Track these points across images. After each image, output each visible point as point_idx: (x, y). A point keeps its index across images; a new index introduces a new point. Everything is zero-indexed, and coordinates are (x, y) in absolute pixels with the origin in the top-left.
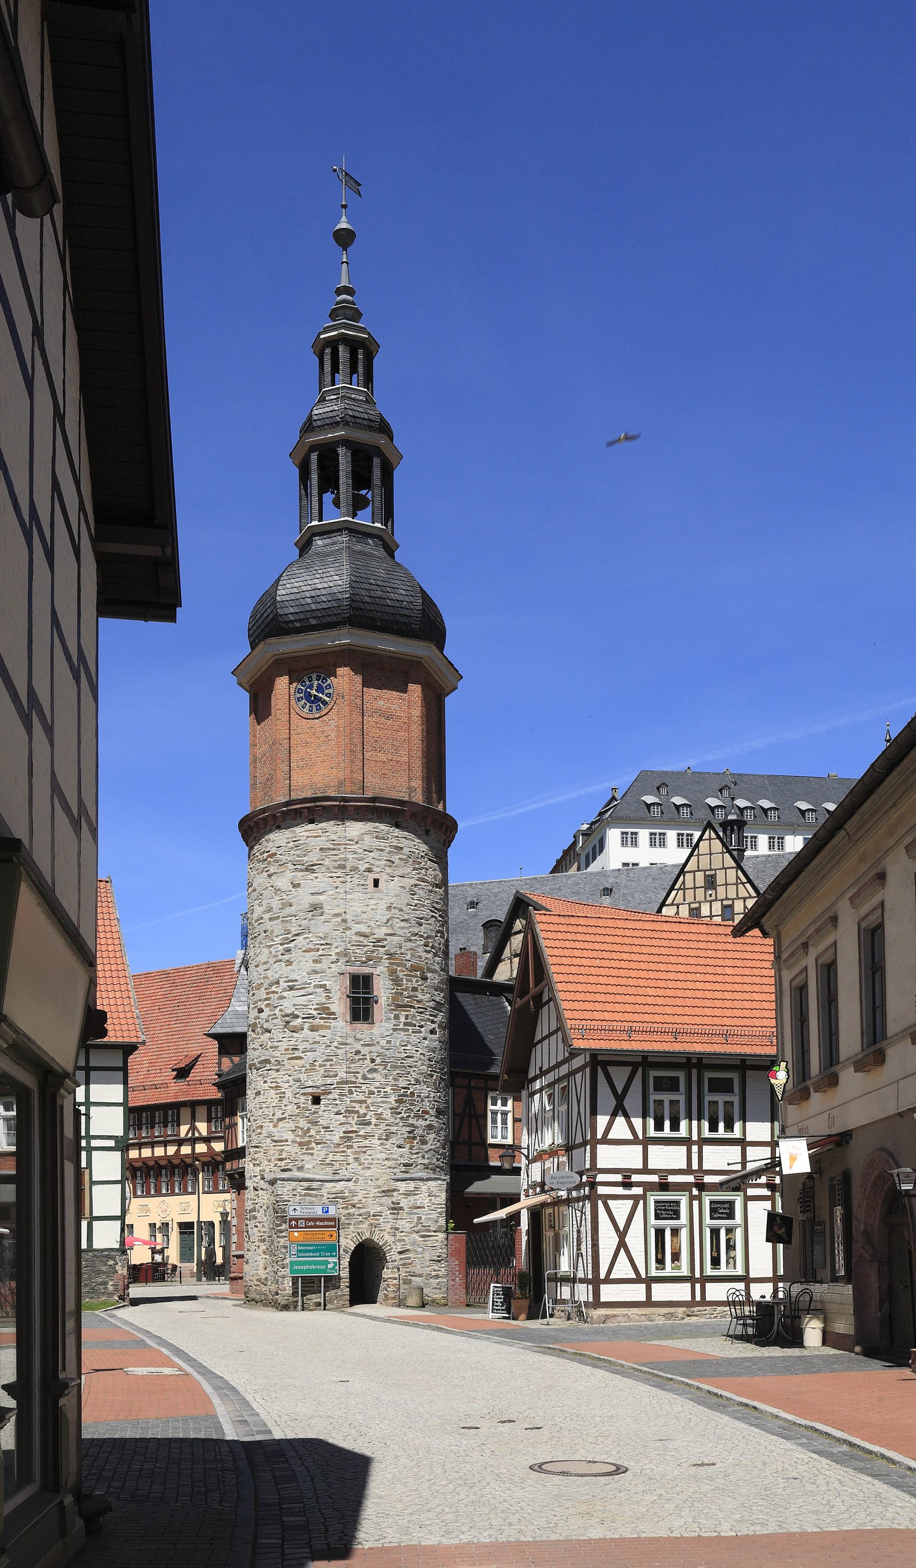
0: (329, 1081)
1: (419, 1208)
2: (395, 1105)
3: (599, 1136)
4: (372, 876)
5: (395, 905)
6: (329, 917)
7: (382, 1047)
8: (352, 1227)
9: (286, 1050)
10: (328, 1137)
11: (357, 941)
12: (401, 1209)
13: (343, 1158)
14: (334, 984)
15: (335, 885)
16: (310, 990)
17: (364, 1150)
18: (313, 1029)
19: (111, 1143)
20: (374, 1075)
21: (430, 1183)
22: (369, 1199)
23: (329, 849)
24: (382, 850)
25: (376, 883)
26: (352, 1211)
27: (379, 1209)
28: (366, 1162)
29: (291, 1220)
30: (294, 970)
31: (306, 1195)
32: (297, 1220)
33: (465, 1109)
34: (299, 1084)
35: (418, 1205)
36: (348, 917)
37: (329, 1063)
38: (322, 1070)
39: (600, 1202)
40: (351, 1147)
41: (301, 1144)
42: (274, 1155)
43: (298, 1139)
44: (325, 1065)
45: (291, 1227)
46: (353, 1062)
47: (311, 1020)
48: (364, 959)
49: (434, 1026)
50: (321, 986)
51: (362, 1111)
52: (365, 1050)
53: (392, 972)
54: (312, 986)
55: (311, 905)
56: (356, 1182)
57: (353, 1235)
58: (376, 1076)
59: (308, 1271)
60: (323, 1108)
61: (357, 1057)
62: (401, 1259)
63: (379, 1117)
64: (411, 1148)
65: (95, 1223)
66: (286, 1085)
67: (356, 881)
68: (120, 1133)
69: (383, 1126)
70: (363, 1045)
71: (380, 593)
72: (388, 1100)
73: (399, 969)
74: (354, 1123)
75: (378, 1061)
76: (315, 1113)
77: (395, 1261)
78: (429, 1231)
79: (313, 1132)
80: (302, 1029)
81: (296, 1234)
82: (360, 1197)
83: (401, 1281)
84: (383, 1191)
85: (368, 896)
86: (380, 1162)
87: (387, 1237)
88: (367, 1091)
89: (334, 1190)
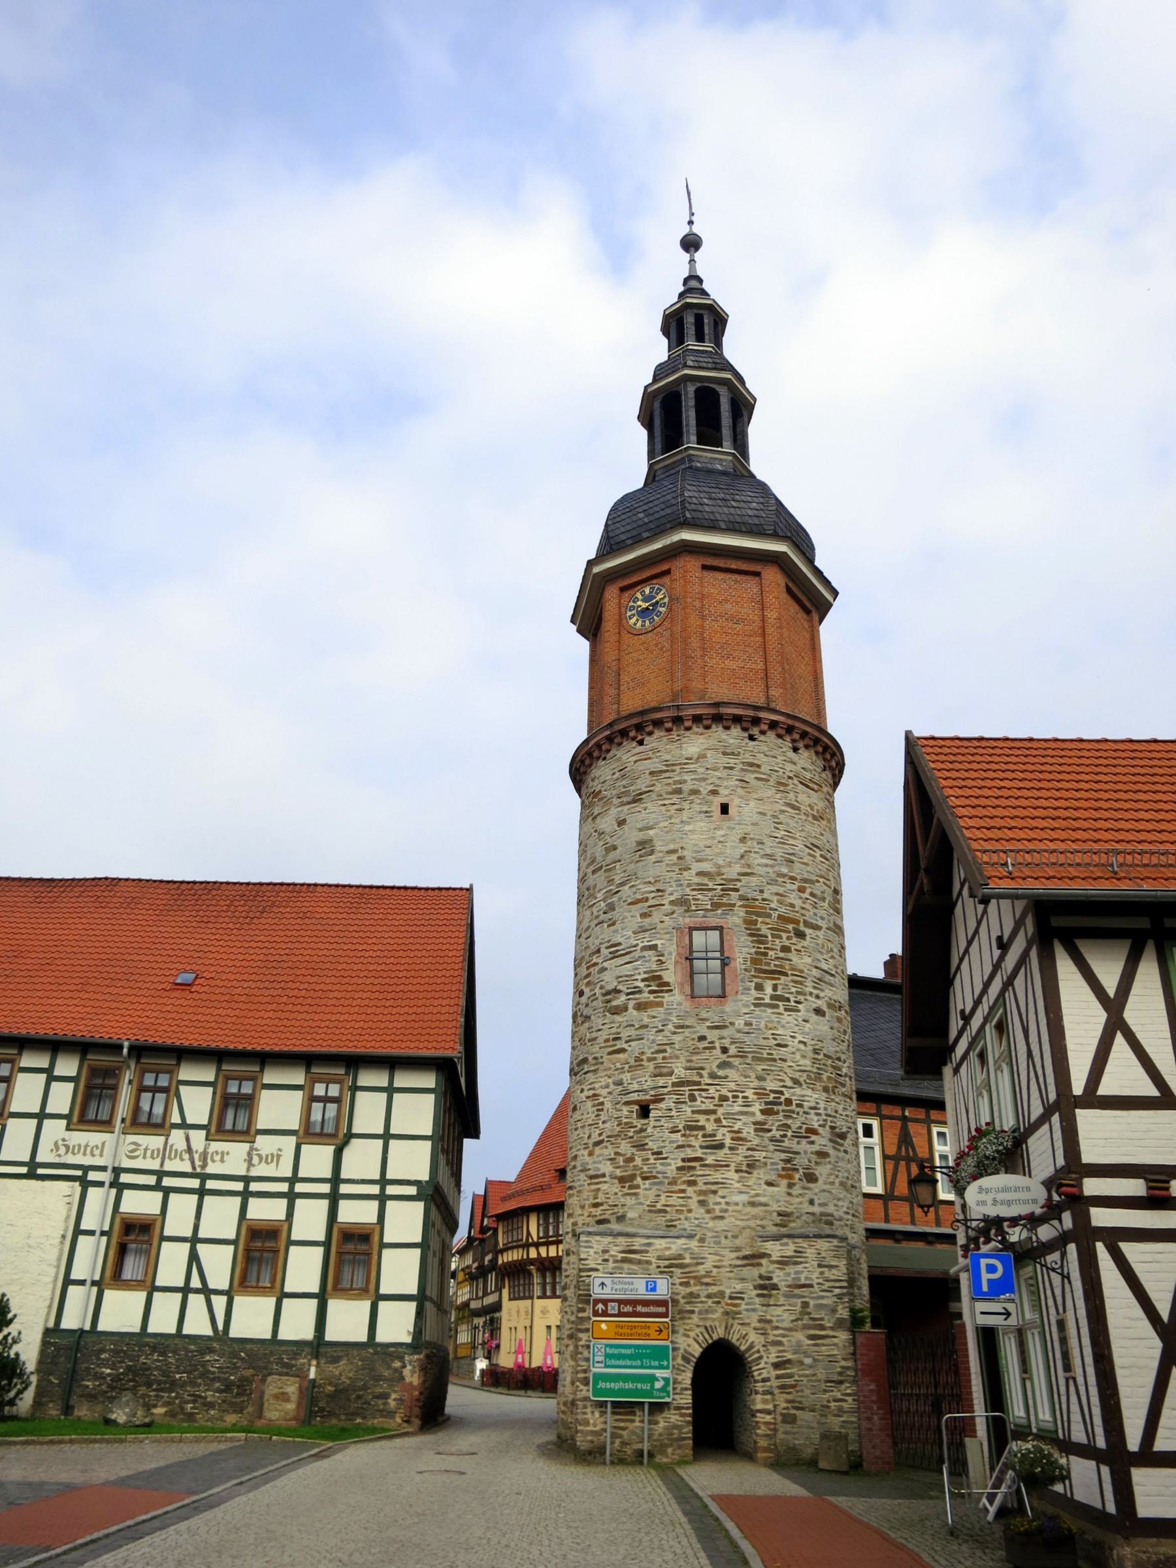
0: (661, 1081)
1: (804, 1286)
2: (760, 1117)
3: (1078, 1088)
4: (717, 801)
7: (739, 1031)
8: (695, 1317)
9: (607, 1041)
10: (660, 1168)
11: (698, 884)
12: (775, 1287)
13: (681, 1201)
14: (668, 944)
16: (637, 954)
17: (714, 1188)
18: (640, 1007)
19: (412, 1190)
22: (722, 1270)
23: (662, 772)
24: (731, 768)
25: (725, 809)
26: (695, 1289)
27: (739, 1287)
28: (717, 1208)
29: (596, 1302)
30: (617, 931)
31: (624, 1260)
32: (605, 1302)
33: (899, 1148)
34: (620, 1088)
35: (803, 1281)
36: (685, 853)
37: (661, 1055)
38: (651, 1066)
39: (1100, 1246)
41: (622, 1180)
42: (588, 1199)
43: (618, 1173)
44: (655, 1059)
45: (596, 1314)
46: (696, 1052)
47: (637, 996)
49: (819, 1002)
52: (712, 1035)
53: (750, 923)
54: (638, 948)
56: (702, 1240)
57: (698, 1331)
59: (621, 1392)
60: (652, 1123)
62: (778, 1377)
63: (738, 1138)
64: (790, 1186)
65: (285, 1301)
66: (604, 1092)
67: (697, 808)
68: (424, 1176)
69: (742, 1150)
70: (709, 1027)
72: (749, 1109)
73: (760, 920)
75: (733, 1050)
78: (822, 1328)
79: (638, 1161)
80: (626, 1009)
81: (604, 1326)
82: (708, 1265)
83: (779, 1418)
84: (745, 1258)
86: (739, 1208)
87: (753, 1337)
88: (716, 1095)
89: (667, 1253)
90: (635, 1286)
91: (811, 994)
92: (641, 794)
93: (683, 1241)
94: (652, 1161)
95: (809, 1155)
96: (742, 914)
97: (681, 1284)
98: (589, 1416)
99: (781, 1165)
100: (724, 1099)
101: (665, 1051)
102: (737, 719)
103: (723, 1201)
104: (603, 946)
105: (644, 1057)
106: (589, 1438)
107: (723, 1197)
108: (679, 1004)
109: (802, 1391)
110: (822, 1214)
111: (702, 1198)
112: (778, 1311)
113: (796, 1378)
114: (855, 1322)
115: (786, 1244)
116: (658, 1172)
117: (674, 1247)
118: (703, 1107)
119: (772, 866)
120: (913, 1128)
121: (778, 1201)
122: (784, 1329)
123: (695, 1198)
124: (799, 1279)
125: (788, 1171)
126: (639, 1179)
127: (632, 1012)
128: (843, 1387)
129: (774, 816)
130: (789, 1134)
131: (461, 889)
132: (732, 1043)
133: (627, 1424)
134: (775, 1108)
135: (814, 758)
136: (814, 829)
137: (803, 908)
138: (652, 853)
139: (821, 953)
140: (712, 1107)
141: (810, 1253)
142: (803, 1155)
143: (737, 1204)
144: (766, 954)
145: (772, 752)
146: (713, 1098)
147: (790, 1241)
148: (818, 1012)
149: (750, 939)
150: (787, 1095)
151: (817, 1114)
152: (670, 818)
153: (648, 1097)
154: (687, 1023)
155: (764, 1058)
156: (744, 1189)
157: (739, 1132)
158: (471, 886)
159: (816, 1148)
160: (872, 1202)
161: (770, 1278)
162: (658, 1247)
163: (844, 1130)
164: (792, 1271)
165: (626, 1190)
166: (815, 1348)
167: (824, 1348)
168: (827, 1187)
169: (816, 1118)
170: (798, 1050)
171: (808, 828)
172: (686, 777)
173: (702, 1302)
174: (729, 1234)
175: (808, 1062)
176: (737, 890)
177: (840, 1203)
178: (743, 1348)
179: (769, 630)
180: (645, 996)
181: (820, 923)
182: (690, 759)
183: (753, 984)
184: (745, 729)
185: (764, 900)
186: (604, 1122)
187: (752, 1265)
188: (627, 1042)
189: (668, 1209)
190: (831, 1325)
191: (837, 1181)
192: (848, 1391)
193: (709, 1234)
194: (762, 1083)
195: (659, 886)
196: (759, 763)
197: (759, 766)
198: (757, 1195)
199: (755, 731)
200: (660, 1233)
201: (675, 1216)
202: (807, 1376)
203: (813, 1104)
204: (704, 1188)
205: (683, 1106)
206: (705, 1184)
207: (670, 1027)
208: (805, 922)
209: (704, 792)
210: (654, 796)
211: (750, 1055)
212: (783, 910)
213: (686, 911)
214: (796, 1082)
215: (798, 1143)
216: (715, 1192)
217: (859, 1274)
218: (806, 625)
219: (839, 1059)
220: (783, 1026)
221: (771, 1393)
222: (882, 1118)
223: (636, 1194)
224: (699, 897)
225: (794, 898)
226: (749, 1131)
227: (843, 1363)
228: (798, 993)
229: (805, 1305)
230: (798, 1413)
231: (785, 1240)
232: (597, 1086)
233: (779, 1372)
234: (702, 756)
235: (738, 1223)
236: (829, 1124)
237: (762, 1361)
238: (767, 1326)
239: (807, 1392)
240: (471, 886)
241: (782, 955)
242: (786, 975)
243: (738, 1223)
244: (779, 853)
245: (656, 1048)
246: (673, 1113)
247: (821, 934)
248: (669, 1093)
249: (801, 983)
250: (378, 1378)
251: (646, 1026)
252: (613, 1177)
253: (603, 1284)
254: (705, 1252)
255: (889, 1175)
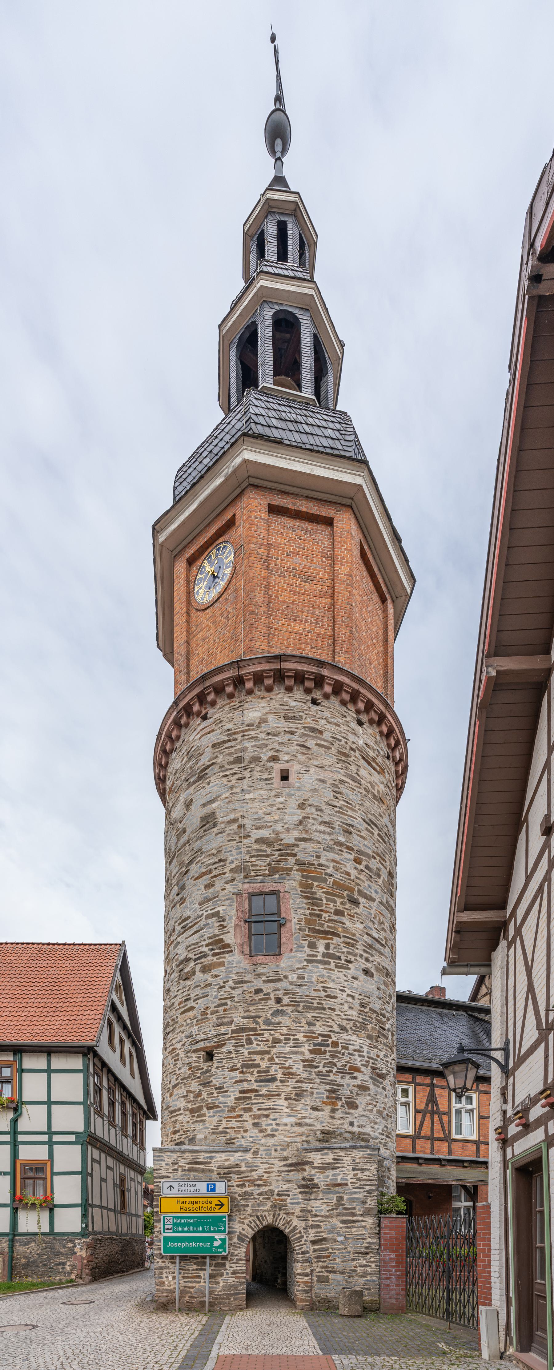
0: (223, 1030)
2: (308, 1056)
4: (278, 767)
5: (310, 802)
6: (222, 826)
7: (292, 983)
10: (221, 1099)
11: (257, 851)
12: (316, 1186)
13: (238, 1124)
15: (230, 784)
16: (202, 923)
17: (266, 1113)
18: (205, 970)
19: (72, 1138)
20: (280, 1019)
21: (355, 1153)
22: (272, 1175)
24: (292, 733)
25: (285, 778)
26: (249, 1189)
28: (269, 1128)
31: (190, 1170)
33: (427, 1105)
34: (190, 1039)
35: (339, 1181)
36: (245, 821)
38: (214, 1017)
40: (250, 1110)
41: (192, 1111)
43: (190, 1106)
44: (217, 1011)
46: (253, 1003)
47: (203, 960)
48: (267, 872)
49: (369, 965)
50: (213, 915)
51: (264, 1065)
52: (268, 988)
54: (204, 917)
55: (203, 819)
56: (256, 1153)
58: (284, 1020)
60: (215, 1065)
61: (257, 997)
62: (315, 1251)
63: (289, 1074)
64: (333, 1111)
68: (81, 1128)
69: (292, 1083)
70: (264, 981)
71: (294, 416)
73: (316, 884)
74: (253, 1079)
75: (286, 1000)
76: (207, 1071)
77: (307, 1252)
78: (354, 1215)
79: (204, 1095)
82: (260, 1172)
83: (315, 1279)
85: (273, 793)
86: (288, 1127)
87: (295, 1222)
88: (270, 1038)
89: (227, 1163)
90: (198, 1188)
91: (361, 956)
92: (205, 769)
93: (240, 1154)
94: (215, 1095)
95: (351, 1087)
96: (298, 878)
97: (238, 1186)
98: (164, 1279)
99: (326, 1094)
100: (276, 1041)
101: (226, 1004)
102: (300, 678)
103: (274, 1122)
104: (177, 924)
105: (209, 1012)
106: (165, 1294)
107: (275, 1120)
108: (239, 962)
109: (335, 1260)
110: (360, 1133)
111: (256, 1121)
112: (318, 1203)
113: (330, 1250)
114: (381, 1212)
115: (327, 1154)
116: (220, 1103)
117: (232, 1159)
118: (259, 1049)
119: (329, 834)
120: (438, 1092)
121: (322, 1123)
122: (322, 1216)
123: (251, 1122)
124: (337, 1179)
125: (333, 1096)
126: (205, 1109)
127: (199, 975)
128: (368, 1257)
129: (335, 786)
130: (335, 1070)
131: (116, 944)
132: (285, 994)
133: (194, 1285)
134: (323, 1048)
135: (378, 738)
136: (375, 808)
137: (358, 878)
138: (215, 825)
139: (374, 923)
140: (266, 1048)
141: (347, 1160)
142: (345, 1087)
143: (286, 1125)
144: (320, 916)
145: (334, 718)
146: (268, 1041)
147: (330, 1152)
148: (366, 972)
149: (305, 901)
150: (334, 1039)
151: (360, 1056)
152: (232, 788)
153: (212, 1044)
154: (245, 979)
155: (317, 1007)
156: (292, 1113)
157: (289, 1068)
158: (124, 942)
159: (358, 1082)
160: (404, 1140)
161: (313, 1180)
162: (219, 1159)
163: (384, 1071)
164: (331, 1174)
165: (195, 1119)
166: (347, 1230)
167: (353, 1230)
168: (364, 1113)
169: (359, 1059)
170: (347, 1002)
171: (368, 804)
172: (248, 744)
173: (255, 1198)
174: (279, 1148)
175: (355, 1013)
176: (295, 855)
177: (376, 1126)
178: (287, 1231)
179: (339, 588)
180: (210, 959)
181: (374, 895)
182: (252, 725)
183: (307, 942)
184: (308, 691)
185: (320, 865)
186: (179, 1069)
187: (298, 1171)
188: (194, 1001)
189: (228, 1130)
190: (361, 1213)
191: (375, 1109)
192: (372, 1259)
193: (262, 1148)
194: (311, 1028)
195: (222, 856)
196: (321, 729)
197: (321, 732)
198: (304, 1118)
199: (318, 695)
200: (221, 1148)
201: (233, 1135)
202: (339, 1249)
203: (357, 1048)
204: (258, 1113)
205: (241, 1048)
206: (259, 1110)
207: (231, 983)
208: (359, 891)
209: (264, 758)
210: (216, 769)
211: (302, 1005)
212: (338, 876)
213: (245, 877)
214: (343, 1028)
215: (342, 1078)
216: (267, 1116)
217: (389, 1178)
218: (380, 612)
219: (384, 1016)
220: (333, 981)
221: (310, 1262)
222: (416, 1084)
223: (203, 1121)
224: (258, 863)
225: (350, 867)
226: (298, 1068)
227: (369, 1240)
228: (348, 953)
229: (341, 1198)
230: (331, 1276)
231: (326, 1151)
232: (174, 1041)
233: (316, 1247)
234: (262, 721)
235: (286, 1139)
236: (371, 1064)
237: (303, 1240)
238: (308, 1215)
239: (338, 1260)
240: (124, 942)
241: (335, 918)
242: (339, 936)
243: (286, 1139)
244: (337, 821)
245: (219, 1002)
246: (233, 1055)
247: (374, 905)
248: (229, 1039)
249: (352, 945)
250: (58, 1254)
251: (211, 985)
252: (185, 1110)
253: (171, 1186)
254: (258, 1161)
255: (418, 1125)
